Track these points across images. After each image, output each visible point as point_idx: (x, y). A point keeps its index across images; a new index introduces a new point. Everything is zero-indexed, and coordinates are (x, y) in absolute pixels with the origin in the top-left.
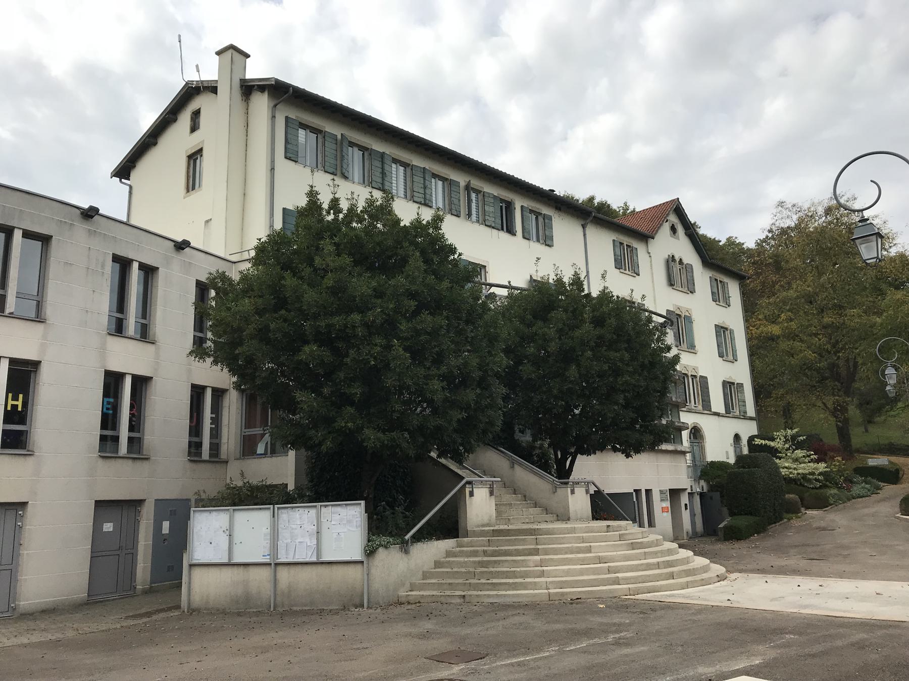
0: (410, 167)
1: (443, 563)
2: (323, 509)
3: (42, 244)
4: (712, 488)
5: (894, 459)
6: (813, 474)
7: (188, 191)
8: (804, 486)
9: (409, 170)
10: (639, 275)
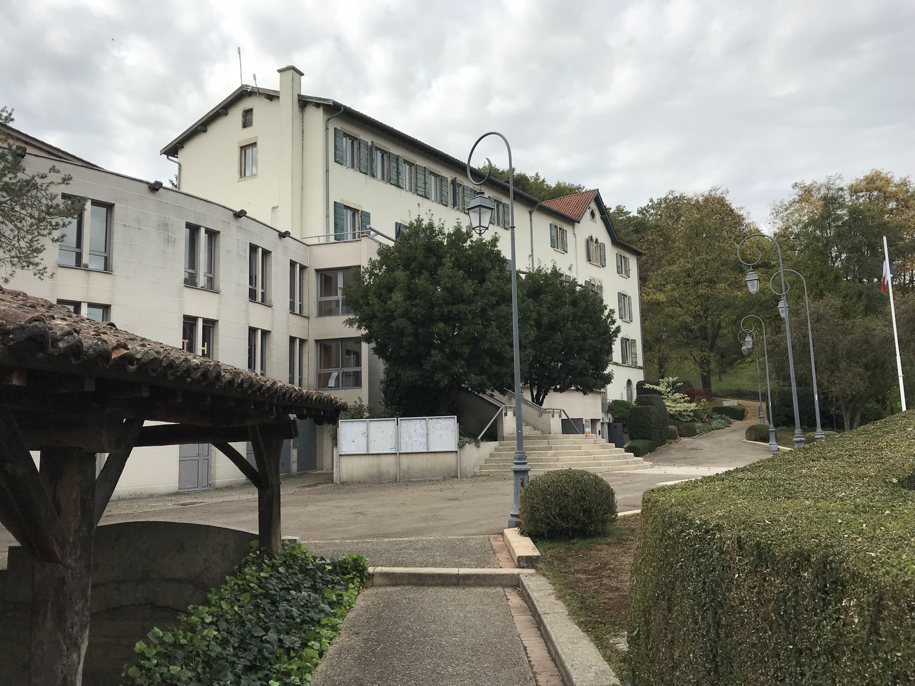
0: (415, 166)
1: (495, 454)
2: (430, 421)
3: (107, 211)
4: (615, 420)
5: (741, 402)
6: (686, 411)
7: (241, 177)
8: (679, 420)
9: (413, 168)
10: (567, 252)
